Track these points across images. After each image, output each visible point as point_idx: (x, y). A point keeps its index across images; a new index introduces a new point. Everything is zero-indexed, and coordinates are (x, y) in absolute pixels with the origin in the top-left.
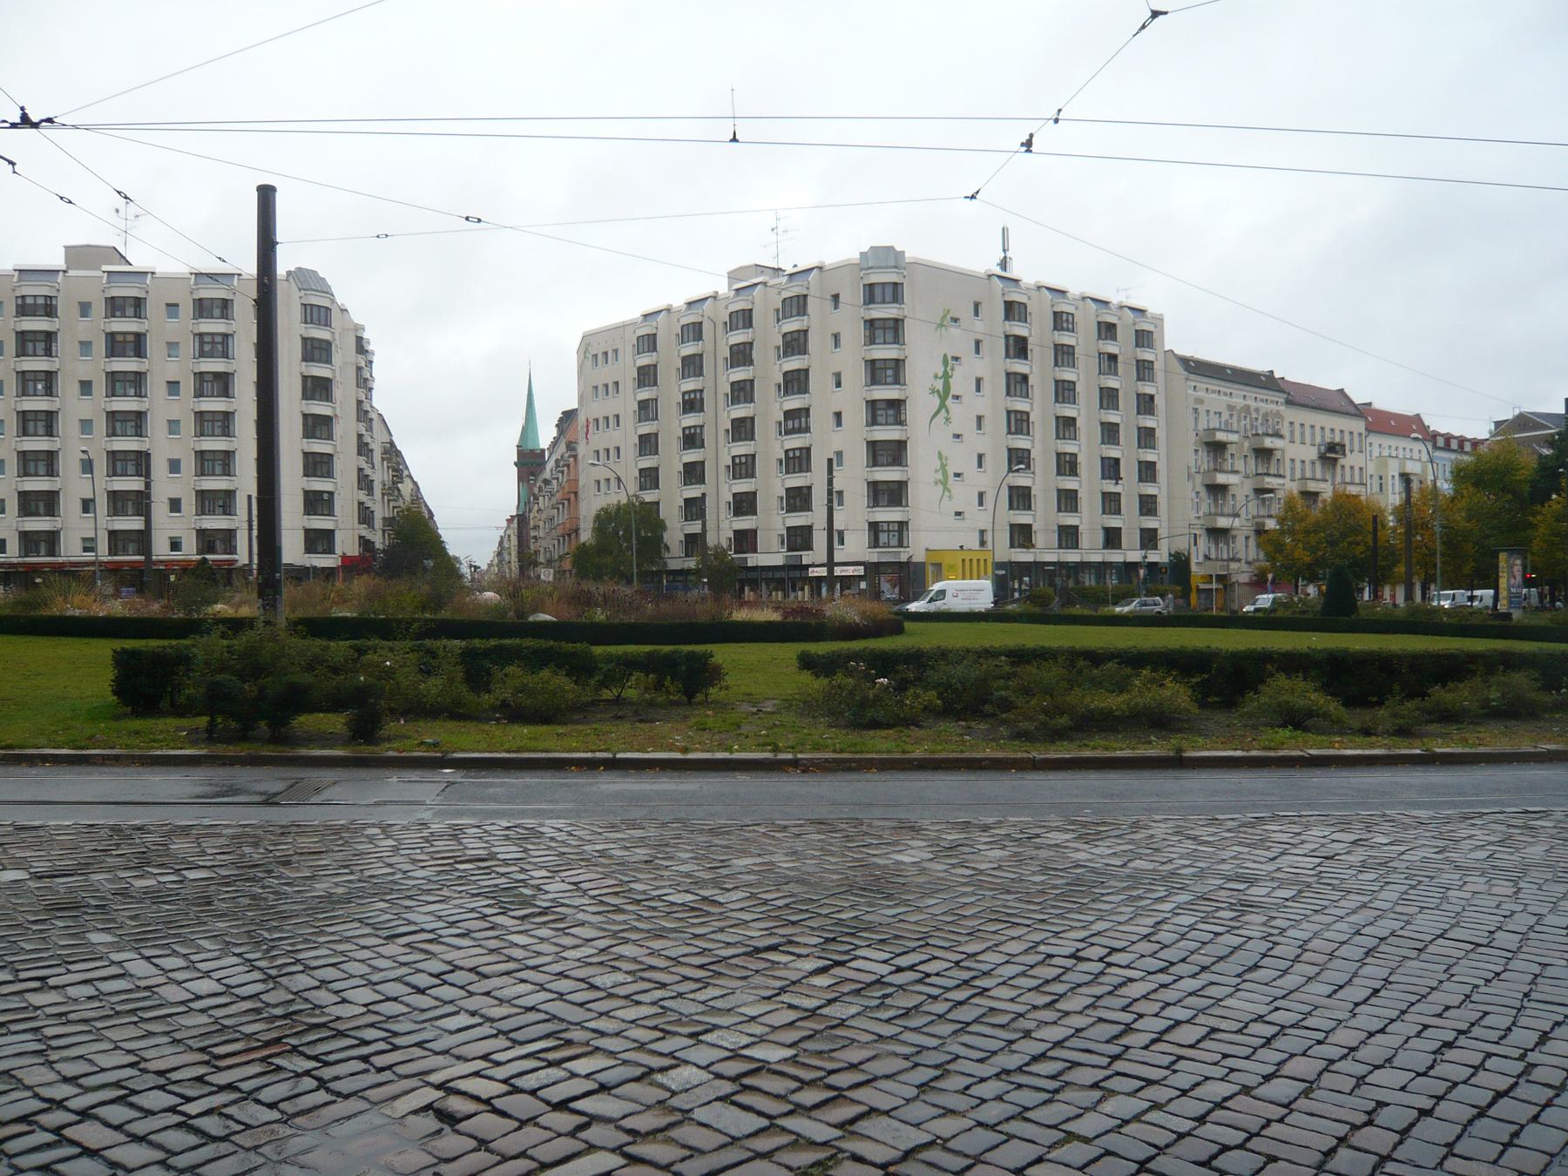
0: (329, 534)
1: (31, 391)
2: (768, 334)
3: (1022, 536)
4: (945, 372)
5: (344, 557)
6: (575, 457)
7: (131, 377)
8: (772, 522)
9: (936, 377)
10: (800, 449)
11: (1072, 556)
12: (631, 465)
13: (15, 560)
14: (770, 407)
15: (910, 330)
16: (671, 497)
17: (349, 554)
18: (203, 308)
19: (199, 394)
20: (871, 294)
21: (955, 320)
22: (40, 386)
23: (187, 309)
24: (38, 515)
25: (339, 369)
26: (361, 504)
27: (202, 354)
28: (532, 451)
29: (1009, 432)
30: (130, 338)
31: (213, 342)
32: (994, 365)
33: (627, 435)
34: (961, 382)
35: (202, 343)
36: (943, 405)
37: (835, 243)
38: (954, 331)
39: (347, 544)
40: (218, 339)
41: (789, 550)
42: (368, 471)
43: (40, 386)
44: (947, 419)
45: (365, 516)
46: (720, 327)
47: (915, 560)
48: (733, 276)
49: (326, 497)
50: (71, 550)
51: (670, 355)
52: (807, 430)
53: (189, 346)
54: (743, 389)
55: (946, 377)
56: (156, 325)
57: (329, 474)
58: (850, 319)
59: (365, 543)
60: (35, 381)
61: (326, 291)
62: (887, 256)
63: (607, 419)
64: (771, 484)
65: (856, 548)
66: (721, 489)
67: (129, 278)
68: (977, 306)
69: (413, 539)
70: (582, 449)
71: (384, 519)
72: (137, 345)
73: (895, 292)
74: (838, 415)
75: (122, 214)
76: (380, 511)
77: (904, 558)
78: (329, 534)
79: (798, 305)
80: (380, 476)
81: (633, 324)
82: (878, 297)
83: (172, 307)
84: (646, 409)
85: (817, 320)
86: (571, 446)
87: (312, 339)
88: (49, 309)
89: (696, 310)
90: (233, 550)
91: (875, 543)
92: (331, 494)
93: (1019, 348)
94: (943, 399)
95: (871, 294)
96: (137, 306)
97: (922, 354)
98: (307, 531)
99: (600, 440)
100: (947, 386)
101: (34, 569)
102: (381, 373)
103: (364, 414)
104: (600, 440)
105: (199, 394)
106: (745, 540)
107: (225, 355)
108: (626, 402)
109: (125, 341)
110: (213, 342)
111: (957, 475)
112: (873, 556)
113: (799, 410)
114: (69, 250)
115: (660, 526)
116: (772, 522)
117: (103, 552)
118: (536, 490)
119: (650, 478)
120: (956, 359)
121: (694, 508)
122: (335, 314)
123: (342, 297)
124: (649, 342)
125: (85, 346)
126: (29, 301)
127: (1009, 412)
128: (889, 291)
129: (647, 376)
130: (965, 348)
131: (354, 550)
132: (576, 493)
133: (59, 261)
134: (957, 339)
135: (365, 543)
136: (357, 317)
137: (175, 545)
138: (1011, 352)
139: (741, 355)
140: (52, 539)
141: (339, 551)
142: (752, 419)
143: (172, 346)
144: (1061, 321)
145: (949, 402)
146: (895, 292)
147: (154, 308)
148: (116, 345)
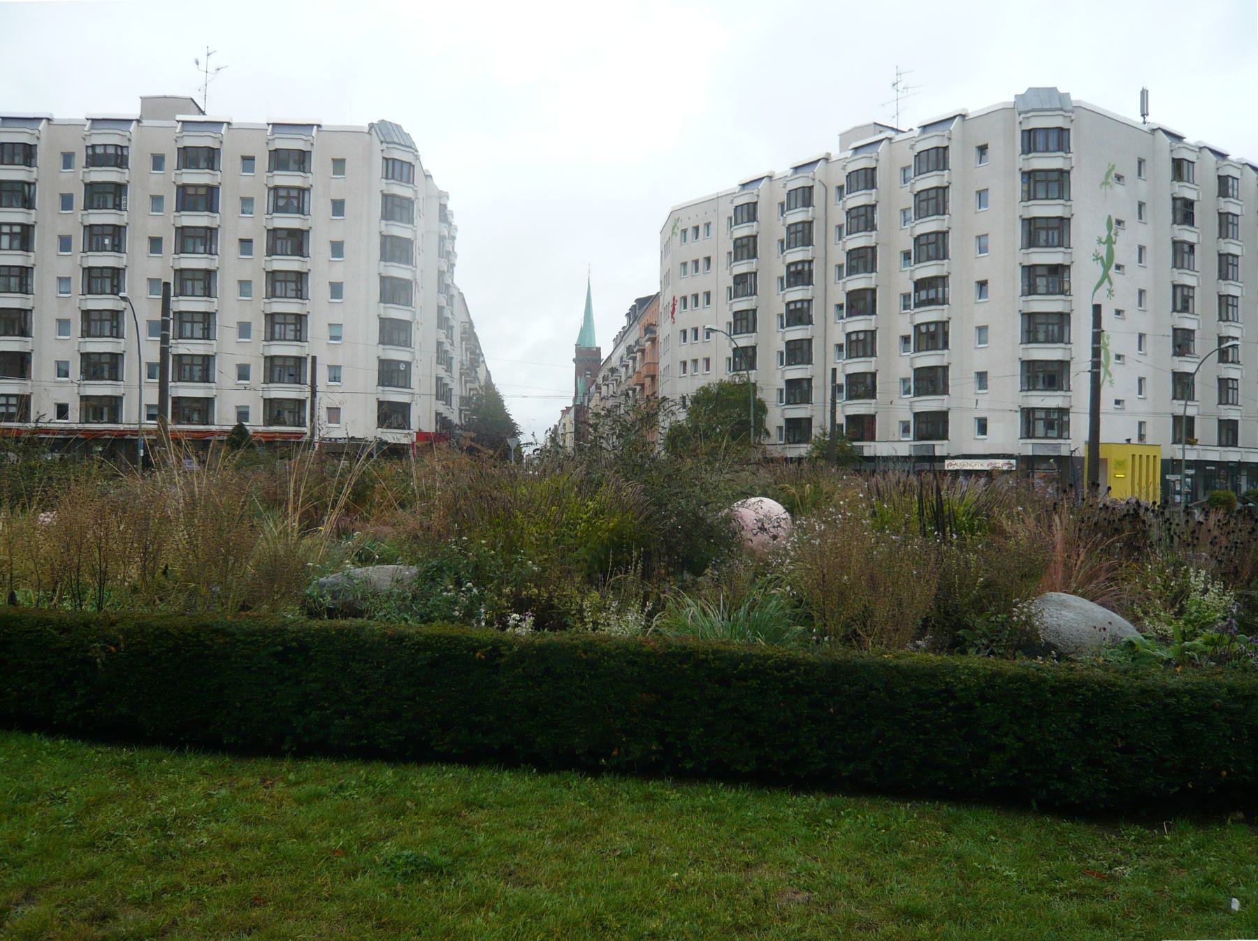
0: (404, 409)
1: (189, 291)
2: (895, 195)
3: (1184, 429)
4: (1109, 237)
5: (421, 435)
6: (654, 341)
7: (202, 233)
8: (895, 409)
9: (1100, 241)
10: (936, 323)
11: (1232, 455)
12: (721, 349)
13: (75, 427)
14: (895, 279)
15: (1077, 184)
16: (771, 377)
17: (425, 430)
18: (280, 160)
19: (271, 251)
20: (1032, 140)
21: (1119, 178)
22: (107, 241)
23: (262, 162)
24: (102, 378)
25: (420, 230)
26: (439, 379)
27: (277, 209)
28: (589, 349)
29: (1174, 310)
30: (202, 191)
31: (288, 197)
32: (1159, 231)
33: (721, 313)
34: (1124, 252)
35: (277, 197)
36: (1106, 275)
37: (984, 87)
38: (1119, 189)
39: (422, 419)
40: (294, 193)
41: (918, 437)
42: (447, 347)
43: (107, 241)
44: (1110, 291)
45: (443, 393)
46: (833, 192)
47: (1077, 454)
48: (845, 137)
49: (402, 367)
50: (43, 412)
51: (772, 227)
52: (945, 302)
53: (263, 201)
54: (858, 258)
55: (1110, 242)
56: (229, 179)
57: (407, 343)
58: (1007, 164)
59: (441, 420)
60: (104, 235)
61: (410, 147)
62: (1052, 99)
63: (696, 297)
64: (896, 364)
65: (1006, 437)
66: (829, 366)
67: (205, 128)
68: (1141, 162)
69: (488, 429)
70: (664, 330)
71: (462, 398)
72: (207, 198)
73: (1060, 139)
74: (982, 284)
75: (202, 65)
76: (457, 390)
77: (1064, 452)
78: (404, 409)
79: (937, 158)
80: (458, 355)
81: (732, 194)
82: (1040, 145)
83: (248, 160)
84: (744, 285)
85: (961, 175)
86: (650, 329)
87: (393, 196)
88: (118, 158)
89: (807, 173)
90: (301, 423)
91: (1028, 433)
92: (408, 364)
93: (1185, 212)
94: (1107, 268)
95: (1032, 140)
96: (210, 158)
97: (1087, 210)
98: (381, 404)
99: (687, 319)
100: (1110, 253)
101: (95, 437)
102: (462, 247)
103: (444, 286)
104: (687, 319)
105: (271, 251)
106: (863, 426)
107: (301, 210)
108: (721, 278)
109: (196, 195)
110: (288, 197)
111: (1118, 357)
112: (1028, 448)
113: (936, 278)
114: (144, 100)
115: (761, 408)
116: (895, 409)
117: (74, 419)
118: (599, 380)
119: (745, 358)
120: (1119, 222)
121: (798, 391)
122: (418, 177)
123: (429, 160)
124: (749, 212)
125: (157, 201)
126: (99, 151)
127: (1175, 287)
128: (1053, 138)
129: (746, 248)
130: (1127, 212)
131: (430, 427)
132: (653, 377)
133: (134, 111)
134: (1121, 201)
135: (441, 420)
136: (440, 182)
137: (62, 411)
138: (1179, 217)
139: (863, 218)
140: (112, 406)
141: (415, 426)
142: (874, 291)
143: (247, 202)
144: (1224, 185)
145: (1112, 271)
146: (1060, 139)
147: (229, 160)
148: (189, 198)
